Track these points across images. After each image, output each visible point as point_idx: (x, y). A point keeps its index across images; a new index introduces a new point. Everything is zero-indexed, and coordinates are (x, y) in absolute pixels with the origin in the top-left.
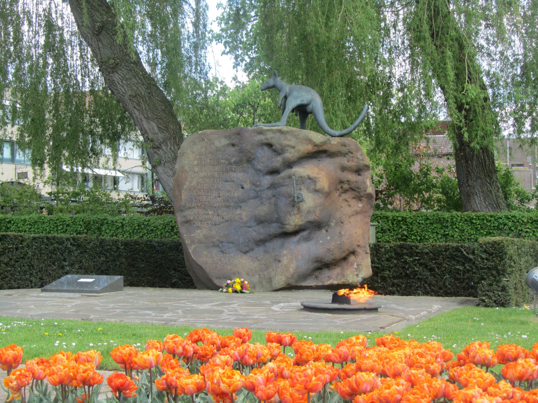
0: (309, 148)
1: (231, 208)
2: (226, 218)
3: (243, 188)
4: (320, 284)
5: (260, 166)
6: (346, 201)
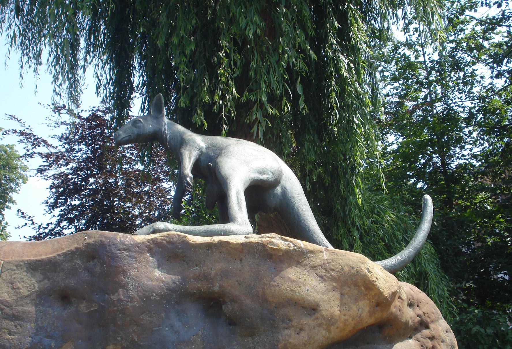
0: (362, 312)
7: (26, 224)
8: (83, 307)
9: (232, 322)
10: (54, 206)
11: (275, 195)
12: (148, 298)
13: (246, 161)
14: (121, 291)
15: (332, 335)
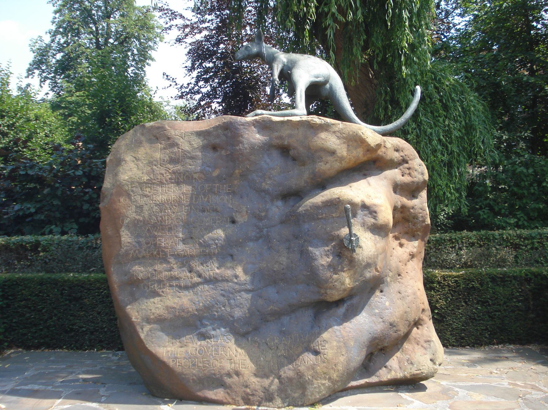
0: (359, 154)
3: (233, 222)
5: (267, 185)
7: (171, 85)
8: (223, 153)
9: (294, 159)
10: (192, 68)
11: (326, 89)
12: (253, 148)
13: (312, 68)
14: (240, 145)
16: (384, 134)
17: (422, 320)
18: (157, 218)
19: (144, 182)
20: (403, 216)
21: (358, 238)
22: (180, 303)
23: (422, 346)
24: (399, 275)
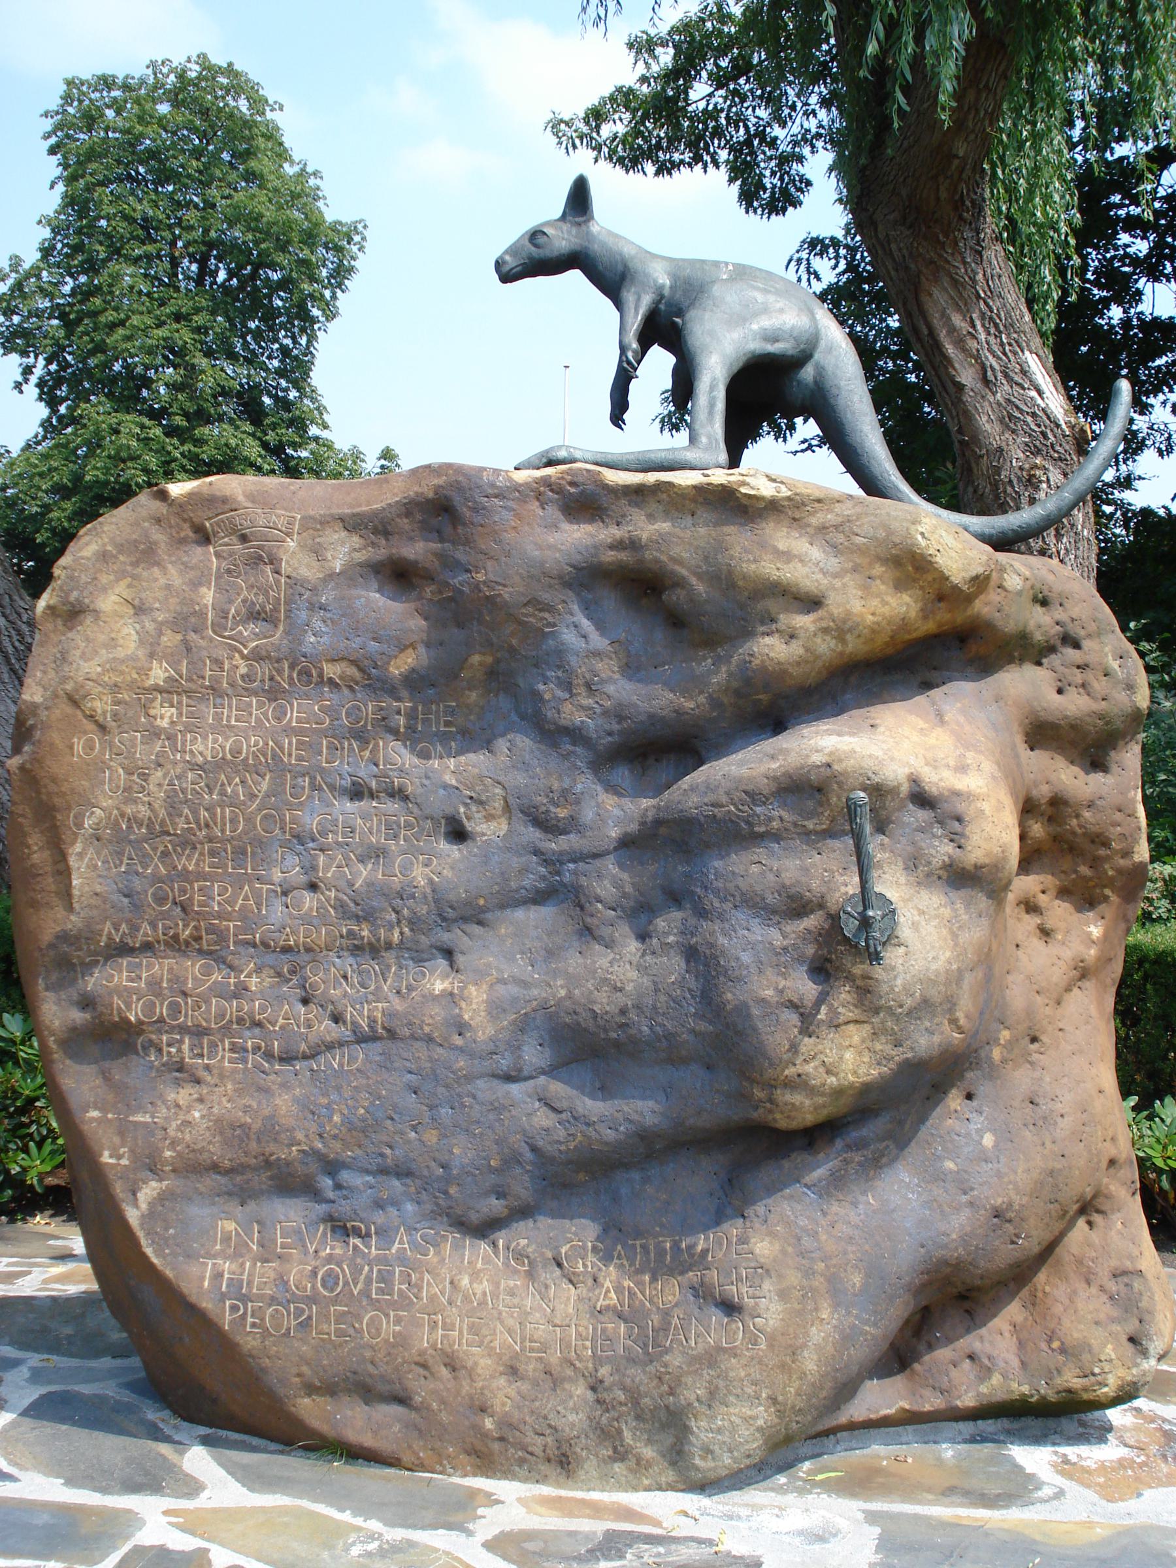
1: (390, 957)
2: (359, 1016)
4: (931, 1402)
6: (1031, 907)
15: (850, 648)
16: (1002, 543)
17: (1108, 1197)
18: (195, 812)
19: (157, 689)
20: (1058, 842)
21: (893, 912)
22: (267, 1112)
23: (1102, 1289)
24: (1034, 1040)
